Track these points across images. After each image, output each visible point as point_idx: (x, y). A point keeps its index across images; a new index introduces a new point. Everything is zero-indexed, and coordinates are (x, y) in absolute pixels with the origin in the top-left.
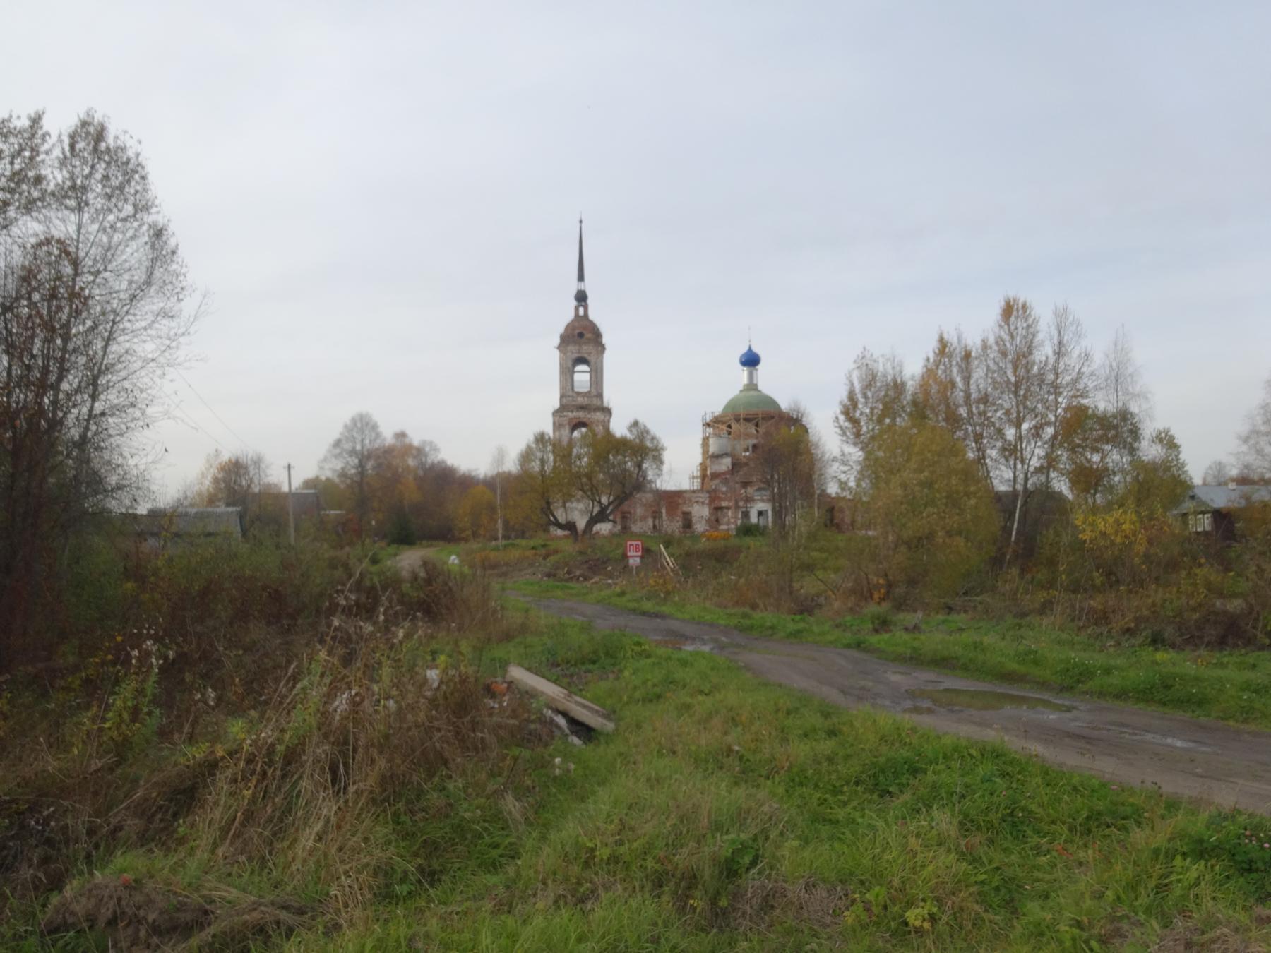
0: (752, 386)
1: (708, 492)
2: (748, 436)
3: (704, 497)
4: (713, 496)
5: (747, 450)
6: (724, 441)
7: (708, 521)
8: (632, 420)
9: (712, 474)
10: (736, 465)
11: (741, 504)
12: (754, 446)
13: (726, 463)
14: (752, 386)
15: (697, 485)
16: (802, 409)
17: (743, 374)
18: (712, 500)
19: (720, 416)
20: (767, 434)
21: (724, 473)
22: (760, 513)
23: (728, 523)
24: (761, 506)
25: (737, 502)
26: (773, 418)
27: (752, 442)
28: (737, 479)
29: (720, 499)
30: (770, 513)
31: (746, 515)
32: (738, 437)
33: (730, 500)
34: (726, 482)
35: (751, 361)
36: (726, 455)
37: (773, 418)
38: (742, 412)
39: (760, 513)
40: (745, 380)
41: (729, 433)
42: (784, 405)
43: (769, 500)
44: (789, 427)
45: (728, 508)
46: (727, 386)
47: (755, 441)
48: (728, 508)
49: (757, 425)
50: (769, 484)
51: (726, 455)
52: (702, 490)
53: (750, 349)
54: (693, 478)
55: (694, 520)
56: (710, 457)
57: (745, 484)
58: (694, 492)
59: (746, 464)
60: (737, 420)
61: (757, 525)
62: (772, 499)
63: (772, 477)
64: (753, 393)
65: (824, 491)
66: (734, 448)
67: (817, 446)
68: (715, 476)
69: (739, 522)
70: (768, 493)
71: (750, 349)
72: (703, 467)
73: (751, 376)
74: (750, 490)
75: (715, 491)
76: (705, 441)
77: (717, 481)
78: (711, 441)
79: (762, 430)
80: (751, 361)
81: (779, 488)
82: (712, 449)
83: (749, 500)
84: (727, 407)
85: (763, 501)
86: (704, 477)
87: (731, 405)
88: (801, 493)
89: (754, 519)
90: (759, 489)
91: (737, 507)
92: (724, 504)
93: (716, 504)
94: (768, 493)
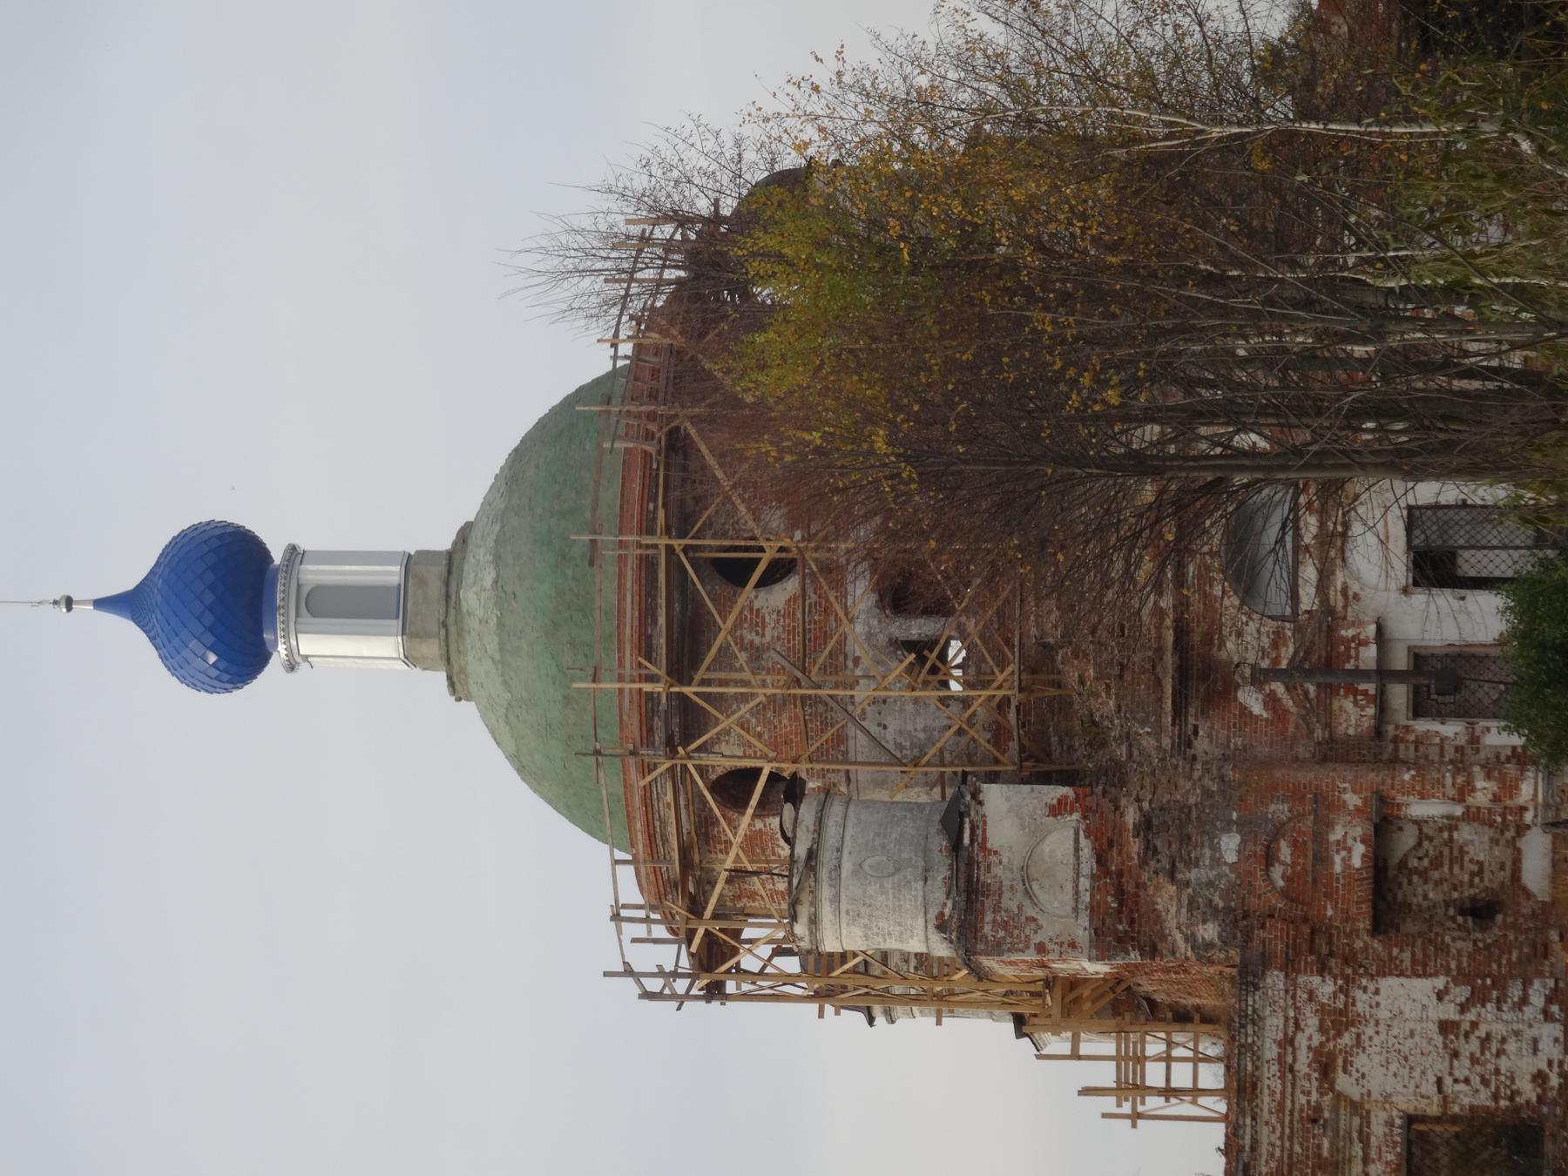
0: (422, 601)
1: (1248, 978)
2: (814, 644)
3: (1287, 1008)
4: (1286, 935)
5: (925, 657)
6: (850, 833)
7: (1484, 984)
8: (291, 675)
9: (1105, 941)
10: (1045, 747)
11: (1353, 716)
12: (898, 597)
13: (1022, 824)
14: (422, 601)
15: (1192, 1064)
16: (620, 218)
17: (335, 669)
18: (1313, 946)
19: (648, 850)
20: (805, 493)
21: (1105, 846)
22: (1434, 567)
23: (1507, 825)
24: (1375, 560)
25: (1335, 751)
26: (676, 444)
27: (860, 614)
28: (1153, 740)
29: (1314, 872)
30: (1427, 492)
31: (1442, 679)
32: (824, 726)
33: (1324, 807)
34: (1176, 835)
35: (221, 601)
36: (958, 827)
37: (676, 444)
38: (621, 686)
39: (1434, 567)
40: (381, 648)
41: (790, 789)
42: (581, 352)
43: (1331, 493)
44: (758, 317)
45: (1383, 823)
46: (425, 834)
47: (861, 594)
48: (1383, 823)
49: (734, 572)
50: (1201, 495)
51: (958, 827)
52: (1235, 1027)
53: (123, 604)
54: (1130, 1088)
55: (1469, 1097)
56: (973, 950)
57: (1200, 678)
58: (1242, 1089)
59: (1040, 663)
60: (687, 723)
61: (1526, 594)
62: (1329, 474)
63: (1142, 464)
64: (476, 597)
65: (1272, 63)
66: (907, 760)
67: (923, 106)
68: (1121, 919)
69: (1499, 738)
70: (1274, 503)
71: (123, 604)
72: (1046, 1007)
73: (346, 606)
74: (1246, 640)
75: (1240, 920)
76: (840, 982)
77: (1167, 901)
78: (840, 935)
79: (773, 534)
80: (221, 601)
81: (1237, 416)
82: (907, 928)
83: (1322, 656)
84: (579, 808)
85: (1333, 544)
86: (1125, 1007)
87: (564, 769)
88: (1283, 244)
89: (1481, 619)
90: (1246, 580)
91: (1378, 748)
92: (1351, 850)
93: (1347, 909)
94: (1274, 503)
